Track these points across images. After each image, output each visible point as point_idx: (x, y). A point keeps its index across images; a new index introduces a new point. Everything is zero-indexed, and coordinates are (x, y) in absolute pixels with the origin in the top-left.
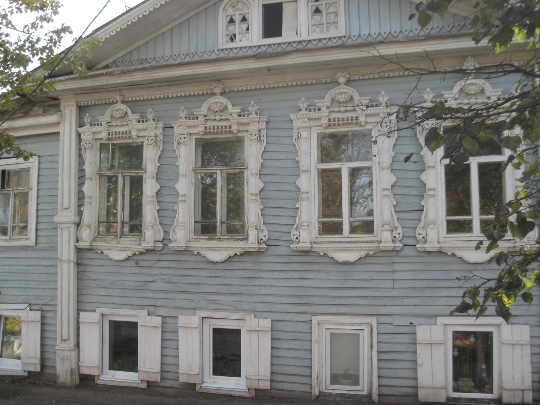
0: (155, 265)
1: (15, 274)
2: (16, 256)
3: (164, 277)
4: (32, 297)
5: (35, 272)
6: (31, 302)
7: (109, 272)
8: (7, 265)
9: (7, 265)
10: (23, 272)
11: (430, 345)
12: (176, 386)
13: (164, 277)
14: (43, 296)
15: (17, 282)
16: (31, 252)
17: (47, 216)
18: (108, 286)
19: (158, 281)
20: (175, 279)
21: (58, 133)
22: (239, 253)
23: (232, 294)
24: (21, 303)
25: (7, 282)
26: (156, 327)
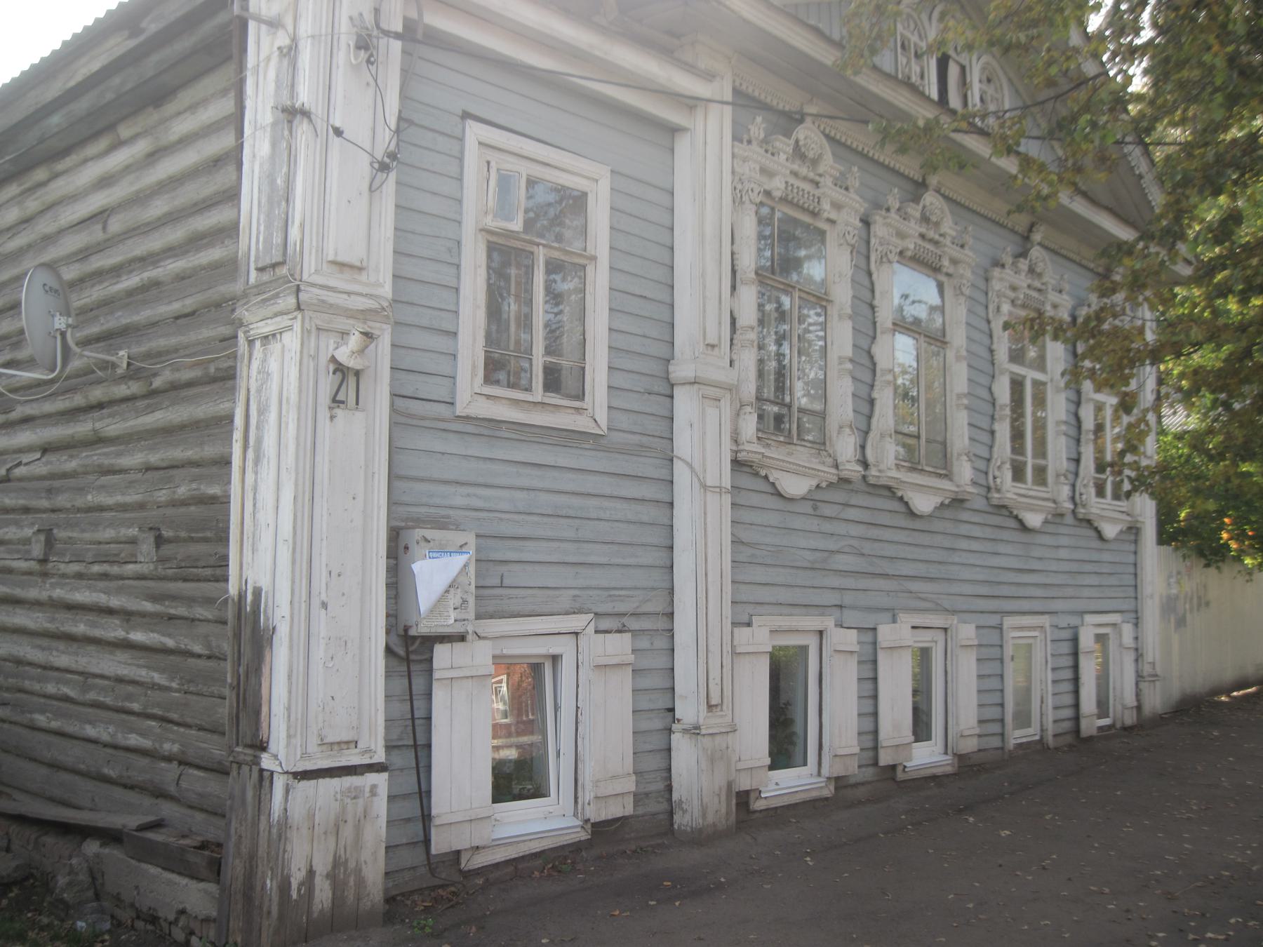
0: (843, 516)
1: (545, 520)
2: (550, 460)
3: (853, 542)
4: (596, 592)
5: (602, 515)
6: (599, 610)
7: (770, 526)
8: (522, 489)
9: (522, 489)
10: (572, 513)
11: (666, 747)
12: (870, 779)
13: (853, 542)
14: (622, 589)
15: (555, 545)
16: (593, 453)
17: (627, 352)
18: (769, 562)
19: (846, 550)
20: (867, 548)
21: (673, 131)
22: (947, 502)
23: (931, 579)
24: (567, 613)
25: (521, 543)
26: (852, 652)
